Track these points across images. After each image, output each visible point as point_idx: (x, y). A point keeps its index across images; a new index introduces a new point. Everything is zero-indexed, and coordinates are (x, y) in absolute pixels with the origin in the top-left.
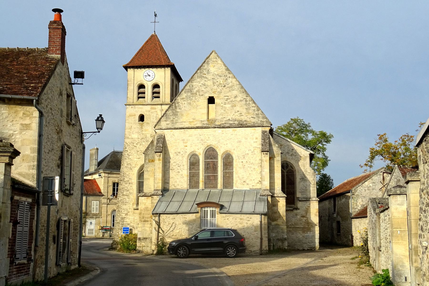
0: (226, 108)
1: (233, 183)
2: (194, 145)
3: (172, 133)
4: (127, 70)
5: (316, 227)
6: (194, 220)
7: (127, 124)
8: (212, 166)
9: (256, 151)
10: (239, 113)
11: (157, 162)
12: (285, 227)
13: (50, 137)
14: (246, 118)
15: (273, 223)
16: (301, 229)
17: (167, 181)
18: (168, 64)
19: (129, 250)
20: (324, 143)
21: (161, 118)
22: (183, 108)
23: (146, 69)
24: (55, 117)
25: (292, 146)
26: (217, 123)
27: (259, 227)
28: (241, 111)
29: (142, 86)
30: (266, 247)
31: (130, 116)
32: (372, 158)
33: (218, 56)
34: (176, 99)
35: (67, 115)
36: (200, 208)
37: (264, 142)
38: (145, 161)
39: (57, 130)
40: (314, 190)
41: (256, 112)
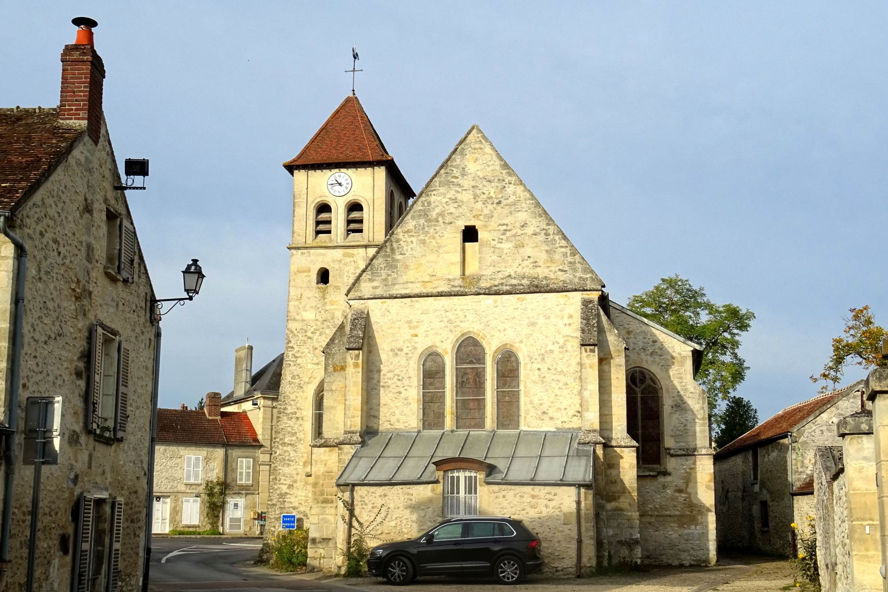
0: (501, 249)
1: (519, 416)
3: (385, 306)
4: (292, 174)
5: (710, 513)
6: (430, 500)
7: (292, 290)
8: (475, 378)
10: (532, 260)
11: (350, 370)
12: (636, 515)
13: (50, 305)
14: (546, 272)
15: (610, 506)
16: (676, 518)
17: (373, 413)
18: (379, 158)
20: (735, 331)
21: (360, 275)
23: (334, 171)
24: (67, 261)
25: (653, 335)
26: (484, 284)
27: (575, 515)
28: (536, 258)
29: (324, 208)
31: (299, 272)
32: (839, 360)
33: (484, 137)
34: (393, 233)
35: (110, 259)
36: (442, 473)
37: (588, 324)
39: (74, 290)
41: (570, 259)
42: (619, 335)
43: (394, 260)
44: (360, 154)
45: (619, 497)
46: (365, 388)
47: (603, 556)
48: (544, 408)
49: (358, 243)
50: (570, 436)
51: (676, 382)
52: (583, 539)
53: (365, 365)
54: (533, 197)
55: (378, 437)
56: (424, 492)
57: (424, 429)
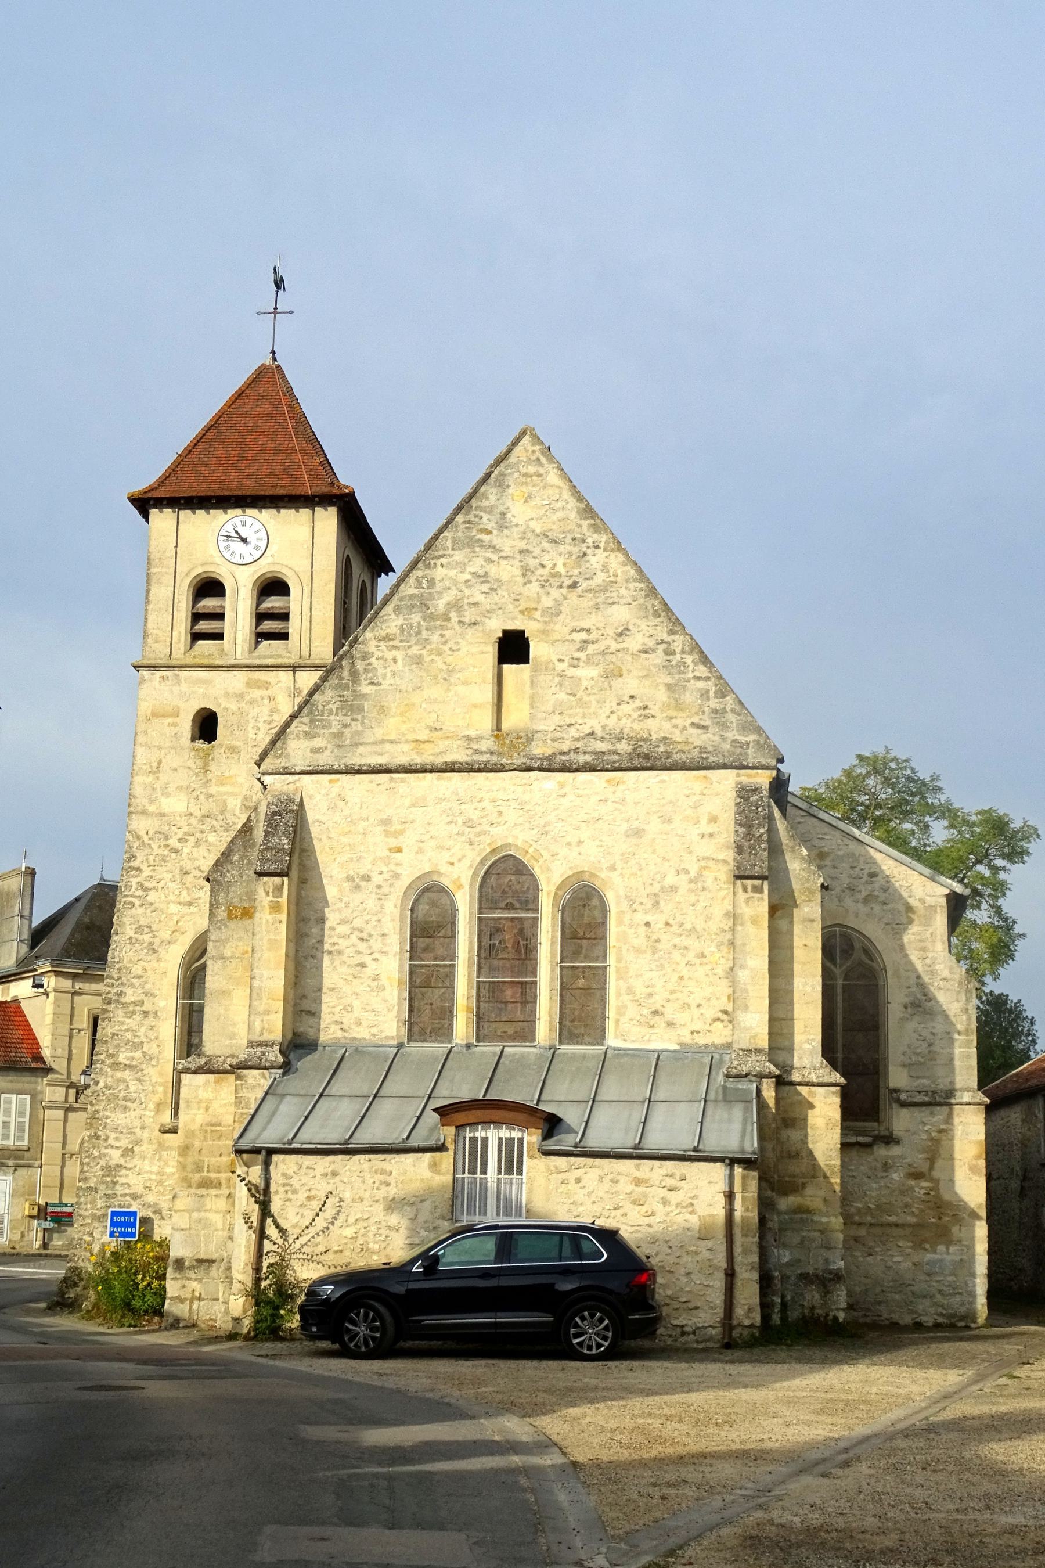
1: (604, 1018)
2: (432, 843)
3: (336, 789)
4: (146, 517)
5: (978, 1223)
7: (140, 751)
8: (513, 944)
9: (709, 877)
10: (638, 703)
12: (836, 1222)
15: (785, 1203)
17: (306, 1005)
18: (325, 489)
19: (134, 1311)
20: (999, 862)
21: (287, 725)
22: (390, 680)
23: (232, 513)
26: (539, 749)
28: (643, 699)
29: (209, 587)
31: (155, 715)
34: (356, 640)
36: (451, 1130)
38: (212, 914)
40: (968, 1057)
41: (714, 703)
42: (810, 860)
43: (357, 695)
44: (285, 481)
46: (292, 954)
47: (772, 1304)
48: (657, 1002)
49: (279, 661)
50: (707, 1060)
51: (914, 956)
52: (736, 1268)
53: (293, 907)
54: (642, 576)
55: (316, 1055)
56: (418, 1173)
57: (409, 1040)
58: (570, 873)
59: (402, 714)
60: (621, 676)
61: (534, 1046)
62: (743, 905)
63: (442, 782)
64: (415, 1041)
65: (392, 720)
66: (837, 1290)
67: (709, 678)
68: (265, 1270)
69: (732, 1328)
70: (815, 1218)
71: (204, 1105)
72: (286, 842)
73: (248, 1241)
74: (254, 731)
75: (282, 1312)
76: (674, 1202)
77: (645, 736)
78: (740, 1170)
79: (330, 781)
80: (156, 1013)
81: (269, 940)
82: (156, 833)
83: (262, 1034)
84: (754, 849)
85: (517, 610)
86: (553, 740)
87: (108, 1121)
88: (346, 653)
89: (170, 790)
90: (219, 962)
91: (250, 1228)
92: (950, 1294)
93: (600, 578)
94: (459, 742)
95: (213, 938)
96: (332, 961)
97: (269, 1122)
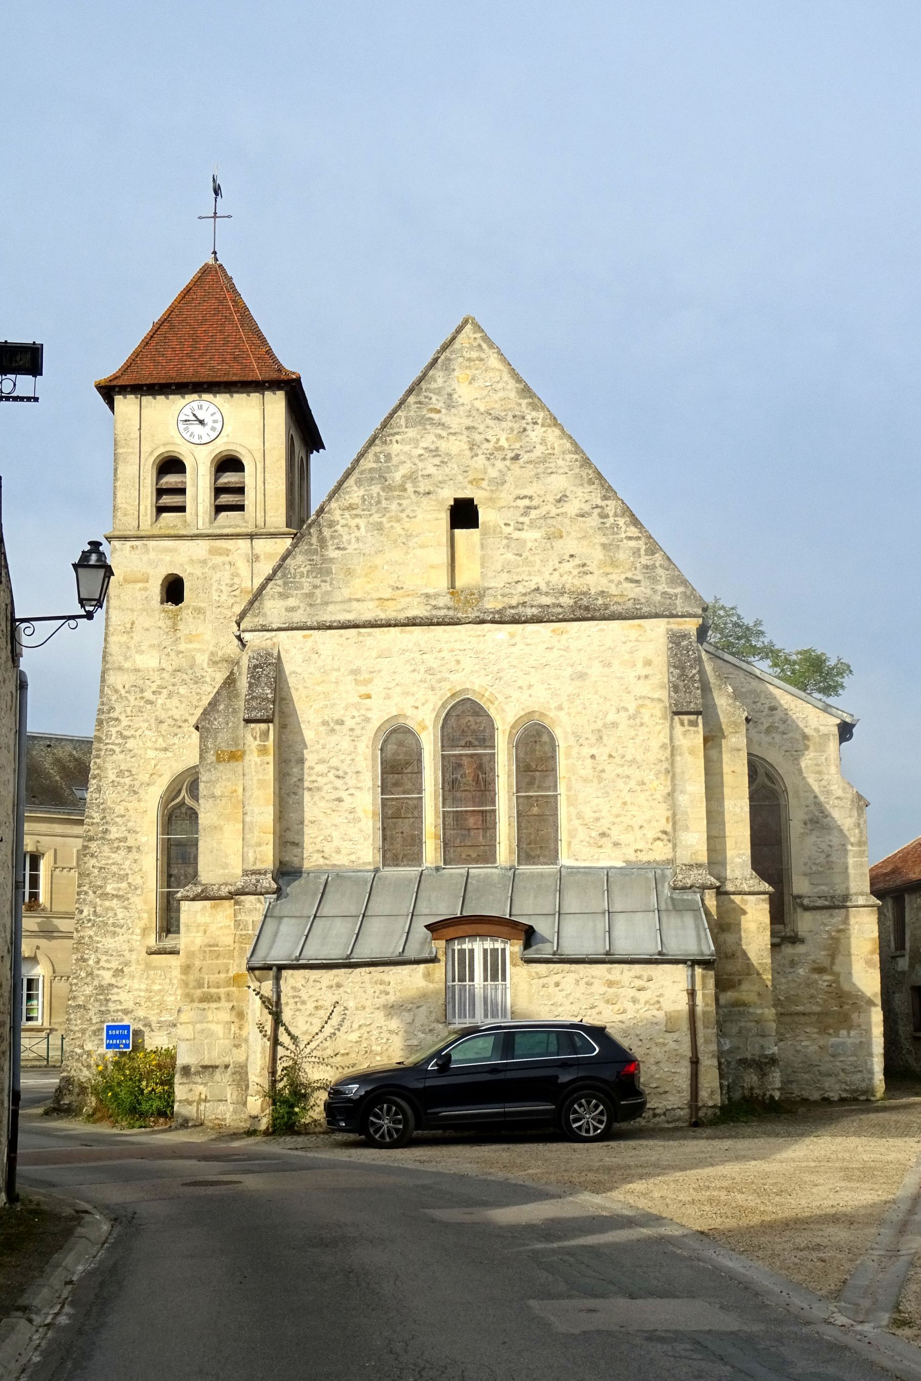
0: (522, 542)
1: (556, 840)
2: (398, 690)
3: (310, 643)
5: (873, 1009)
8: (471, 776)
10: (577, 561)
11: (253, 758)
12: (770, 1013)
16: (814, 1018)
17: (290, 836)
18: (274, 376)
21: (263, 587)
22: (354, 545)
23: (190, 398)
26: (491, 604)
28: (581, 558)
29: (171, 465)
30: (712, 1093)
31: (127, 581)
33: (486, 339)
37: (683, 676)
41: (645, 560)
43: (325, 560)
45: (740, 982)
46: (277, 792)
48: (604, 825)
50: (651, 875)
52: (699, 1055)
54: (577, 449)
55: (302, 881)
56: (412, 980)
57: (384, 865)
58: (522, 713)
59: (366, 575)
60: (561, 537)
61: (496, 867)
62: (681, 737)
63: (403, 635)
64: (389, 866)
65: (357, 581)
66: (774, 1072)
67: (638, 538)
68: (279, 1073)
69: (698, 1109)
70: (751, 1010)
71: (202, 928)
72: (269, 691)
73: (264, 1047)
74: (218, 594)
75: (297, 1110)
76: (642, 1001)
77: (585, 590)
78: (700, 970)
79: (304, 637)
80: (138, 848)
81: (259, 780)
82: (132, 686)
83: (255, 863)
84: (689, 688)
85: (466, 480)
86: (503, 596)
87: (99, 945)
88: (314, 522)
89: (143, 648)
90: (211, 801)
91: (265, 1036)
92: (853, 1072)
93: (539, 450)
94: (419, 599)
95: (204, 779)
96: (312, 797)
97: (273, 942)
